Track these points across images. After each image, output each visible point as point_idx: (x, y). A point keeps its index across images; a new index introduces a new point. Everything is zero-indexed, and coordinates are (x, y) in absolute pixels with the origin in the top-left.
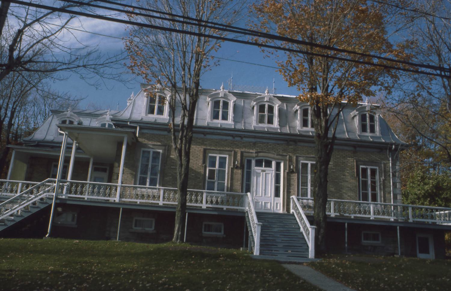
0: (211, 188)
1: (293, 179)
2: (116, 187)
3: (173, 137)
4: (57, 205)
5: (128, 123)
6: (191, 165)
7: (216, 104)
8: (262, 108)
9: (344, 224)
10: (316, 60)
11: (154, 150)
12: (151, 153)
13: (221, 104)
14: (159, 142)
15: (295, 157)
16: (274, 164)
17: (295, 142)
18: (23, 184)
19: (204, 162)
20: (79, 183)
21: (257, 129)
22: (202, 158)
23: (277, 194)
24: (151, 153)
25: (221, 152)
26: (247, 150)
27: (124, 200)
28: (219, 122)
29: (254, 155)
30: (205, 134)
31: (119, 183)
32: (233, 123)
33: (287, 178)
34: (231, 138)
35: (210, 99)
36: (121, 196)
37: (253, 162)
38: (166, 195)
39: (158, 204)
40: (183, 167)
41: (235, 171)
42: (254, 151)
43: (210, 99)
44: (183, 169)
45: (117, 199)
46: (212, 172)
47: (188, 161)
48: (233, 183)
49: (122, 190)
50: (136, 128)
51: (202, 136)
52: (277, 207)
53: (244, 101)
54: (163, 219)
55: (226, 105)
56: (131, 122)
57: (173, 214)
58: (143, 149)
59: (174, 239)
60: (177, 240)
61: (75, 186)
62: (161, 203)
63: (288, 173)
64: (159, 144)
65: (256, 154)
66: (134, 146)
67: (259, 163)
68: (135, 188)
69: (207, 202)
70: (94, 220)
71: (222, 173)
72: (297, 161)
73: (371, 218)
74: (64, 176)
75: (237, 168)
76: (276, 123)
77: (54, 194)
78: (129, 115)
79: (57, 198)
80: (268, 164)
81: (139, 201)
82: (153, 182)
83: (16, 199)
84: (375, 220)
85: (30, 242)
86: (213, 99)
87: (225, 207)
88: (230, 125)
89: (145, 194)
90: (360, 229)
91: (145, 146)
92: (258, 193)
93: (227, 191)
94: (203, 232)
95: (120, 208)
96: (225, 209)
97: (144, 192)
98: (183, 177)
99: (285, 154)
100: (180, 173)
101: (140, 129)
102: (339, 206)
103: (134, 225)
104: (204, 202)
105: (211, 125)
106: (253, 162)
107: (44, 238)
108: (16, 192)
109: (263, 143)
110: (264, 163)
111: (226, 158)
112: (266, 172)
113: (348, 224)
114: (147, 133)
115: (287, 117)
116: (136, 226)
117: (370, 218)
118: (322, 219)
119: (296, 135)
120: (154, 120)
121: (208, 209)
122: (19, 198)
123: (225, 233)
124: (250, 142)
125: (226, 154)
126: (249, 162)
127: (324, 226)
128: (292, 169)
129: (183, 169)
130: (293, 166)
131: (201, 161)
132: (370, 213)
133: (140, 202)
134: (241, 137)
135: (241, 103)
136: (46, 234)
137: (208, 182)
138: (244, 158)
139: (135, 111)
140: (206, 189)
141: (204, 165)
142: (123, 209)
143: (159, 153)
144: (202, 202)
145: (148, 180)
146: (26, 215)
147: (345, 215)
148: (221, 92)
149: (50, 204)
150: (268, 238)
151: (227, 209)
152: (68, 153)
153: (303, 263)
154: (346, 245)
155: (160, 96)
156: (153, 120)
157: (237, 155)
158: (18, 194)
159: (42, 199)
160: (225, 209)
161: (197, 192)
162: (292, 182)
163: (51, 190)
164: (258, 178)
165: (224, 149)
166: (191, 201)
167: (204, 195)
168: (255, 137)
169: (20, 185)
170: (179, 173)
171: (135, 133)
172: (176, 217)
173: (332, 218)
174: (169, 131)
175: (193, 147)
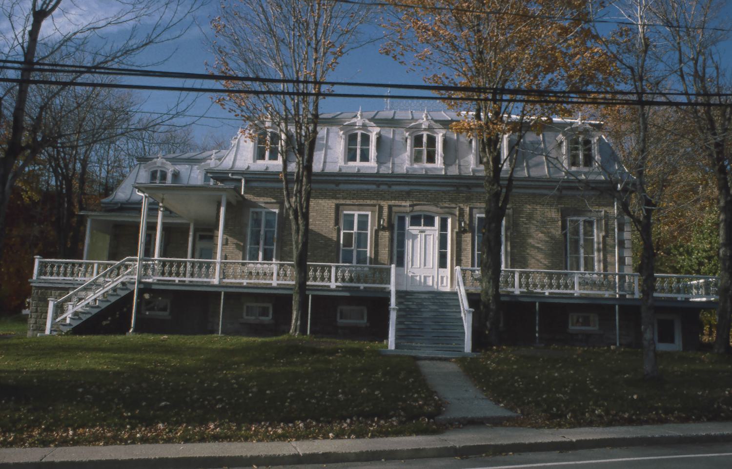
0: (348, 259)
1: (466, 241)
2: (215, 263)
3: (285, 193)
4: (141, 292)
5: (230, 175)
6: (311, 227)
7: (351, 139)
8: (418, 141)
9: (535, 303)
10: (37, 101)
11: (266, 210)
12: (264, 214)
13: (359, 139)
14: (274, 199)
15: (468, 209)
16: (437, 220)
17: (469, 186)
18: (99, 264)
19: (337, 222)
20: (318, 265)
21: (361, 172)
22: (334, 217)
23: (442, 264)
24: (264, 214)
25: (360, 206)
26: (397, 203)
27: (226, 281)
28: (357, 165)
29: (408, 209)
30: (337, 183)
31: (218, 258)
32: (376, 165)
33: (457, 240)
34: (374, 187)
35: (342, 132)
36: (224, 275)
37: (408, 220)
38: (340, 274)
39: (329, 286)
40: (301, 233)
41: (381, 233)
42: (408, 203)
43: (342, 132)
44: (300, 237)
45: (216, 281)
46: (348, 237)
47: (307, 224)
48: (378, 250)
49: (229, 268)
50: (240, 180)
51: (333, 186)
52: (442, 283)
53: (394, 131)
54: (279, 302)
55: (366, 139)
56: (233, 174)
57: (289, 298)
58: (252, 210)
59: (291, 331)
60: (296, 331)
61: (199, 267)
62: (275, 283)
63: (457, 233)
64: (273, 201)
65: (411, 208)
66: (238, 209)
67: (415, 221)
68: (243, 264)
69: (336, 280)
70: (191, 308)
71: (362, 240)
72: (471, 215)
73: (575, 295)
74: (149, 252)
75: (384, 229)
76: (439, 162)
77: (136, 277)
78: (231, 163)
79: (140, 282)
80: (429, 222)
81: (245, 282)
82: (267, 257)
83: (91, 284)
84: (278, 287)
85: (108, 340)
86: (347, 132)
87: (362, 286)
88: (372, 168)
89: (268, 271)
90: (557, 313)
91: (255, 205)
92: (427, 264)
93: (371, 263)
94: (246, 317)
95: (221, 292)
96: (362, 288)
97: (252, 268)
98: (300, 246)
99: (454, 206)
100: (297, 242)
101: (246, 182)
102: (528, 277)
103: (245, 314)
104: (332, 279)
105: (344, 171)
106: (408, 220)
107: (127, 333)
108: (92, 274)
109: (420, 192)
110: (422, 220)
111: (367, 216)
112: (426, 233)
113: (540, 304)
114: (257, 187)
115: (456, 151)
116: (247, 315)
117: (574, 294)
118: (491, 298)
119: (469, 178)
120: (265, 168)
121: (337, 289)
122: (93, 283)
123: (368, 320)
124: (402, 191)
125: (367, 211)
126: (402, 220)
127: (494, 307)
128: (464, 227)
129: (300, 237)
130: (465, 223)
131: (332, 222)
132: (513, 286)
133: (247, 283)
134: (389, 185)
135: (388, 133)
136: (130, 329)
137: (343, 250)
138: (393, 214)
139: (239, 157)
140: (341, 261)
141: (336, 227)
142: (226, 293)
143: (275, 213)
144: (329, 279)
145: (261, 254)
146: (104, 305)
147: (535, 291)
148: (359, 121)
149: (132, 289)
150: (413, 326)
151: (365, 288)
152: (150, 223)
153: (451, 358)
154: (537, 335)
155: (362, 135)
156: (263, 169)
157: (383, 210)
158: (95, 277)
159: (123, 283)
160: (362, 288)
161: (323, 267)
162: (463, 246)
163: (133, 272)
164: (415, 241)
165: (365, 203)
166: (315, 279)
167: (333, 270)
168: (409, 184)
169: (96, 266)
170: (296, 240)
171: (237, 190)
172: (293, 302)
173: (516, 296)
174: (280, 181)
175: (313, 203)
